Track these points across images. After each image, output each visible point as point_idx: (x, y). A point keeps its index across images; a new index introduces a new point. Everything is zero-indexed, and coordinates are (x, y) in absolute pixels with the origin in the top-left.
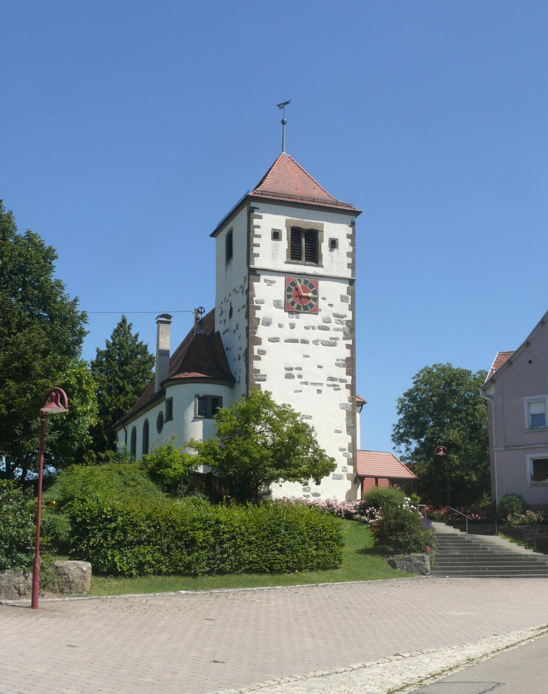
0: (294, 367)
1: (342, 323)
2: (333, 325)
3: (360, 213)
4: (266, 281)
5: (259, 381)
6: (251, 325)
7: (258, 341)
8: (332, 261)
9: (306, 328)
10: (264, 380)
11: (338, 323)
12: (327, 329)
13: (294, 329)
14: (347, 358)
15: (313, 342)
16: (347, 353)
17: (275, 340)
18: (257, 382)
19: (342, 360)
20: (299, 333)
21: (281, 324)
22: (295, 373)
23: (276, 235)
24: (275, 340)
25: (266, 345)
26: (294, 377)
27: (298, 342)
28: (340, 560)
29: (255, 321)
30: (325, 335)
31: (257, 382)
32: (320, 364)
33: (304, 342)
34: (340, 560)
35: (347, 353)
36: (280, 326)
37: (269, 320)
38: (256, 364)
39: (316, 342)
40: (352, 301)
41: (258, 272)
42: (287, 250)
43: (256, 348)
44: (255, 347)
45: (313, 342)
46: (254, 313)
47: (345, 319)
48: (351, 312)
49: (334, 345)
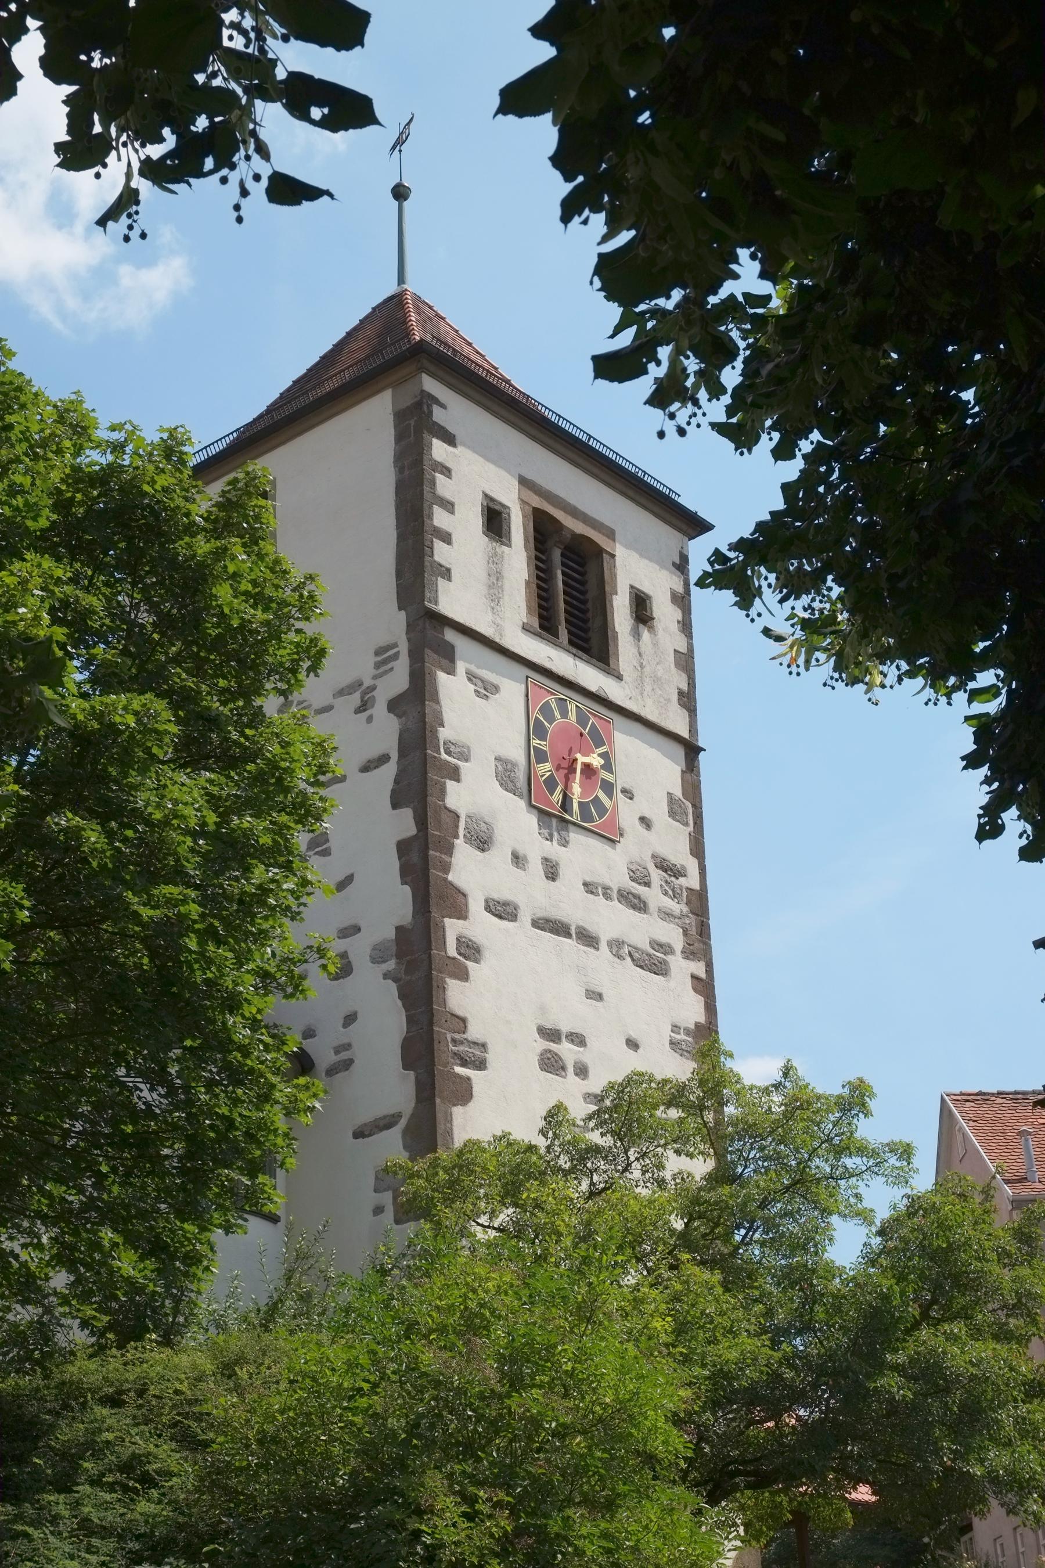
0: (565, 1029)
1: (675, 896)
2: (655, 896)
3: (566, 219)
4: (471, 677)
5: (464, 1064)
6: (433, 832)
7: (456, 904)
8: (642, 666)
9: (589, 887)
10: (481, 1065)
11: (666, 893)
12: (639, 905)
13: (557, 883)
14: (697, 1025)
15: (610, 944)
16: (693, 1012)
17: (503, 910)
18: (459, 1070)
19: (687, 1032)
20: (569, 902)
21: (521, 852)
22: (566, 1050)
23: (494, 520)
24: (503, 910)
25: (479, 925)
26: (563, 1068)
27: (568, 935)
28: (830, 1240)
29: (445, 817)
30: (642, 930)
31: (459, 1070)
32: (634, 1035)
33: (588, 939)
34: (830, 1240)
35: (693, 1012)
36: (518, 859)
37: (484, 827)
38: (457, 996)
39: (616, 946)
40: (695, 823)
41: (450, 635)
42: (527, 583)
43: (453, 928)
44: (448, 921)
45: (610, 944)
46: (443, 791)
47: (682, 881)
48: (696, 861)
49: (659, 969)
